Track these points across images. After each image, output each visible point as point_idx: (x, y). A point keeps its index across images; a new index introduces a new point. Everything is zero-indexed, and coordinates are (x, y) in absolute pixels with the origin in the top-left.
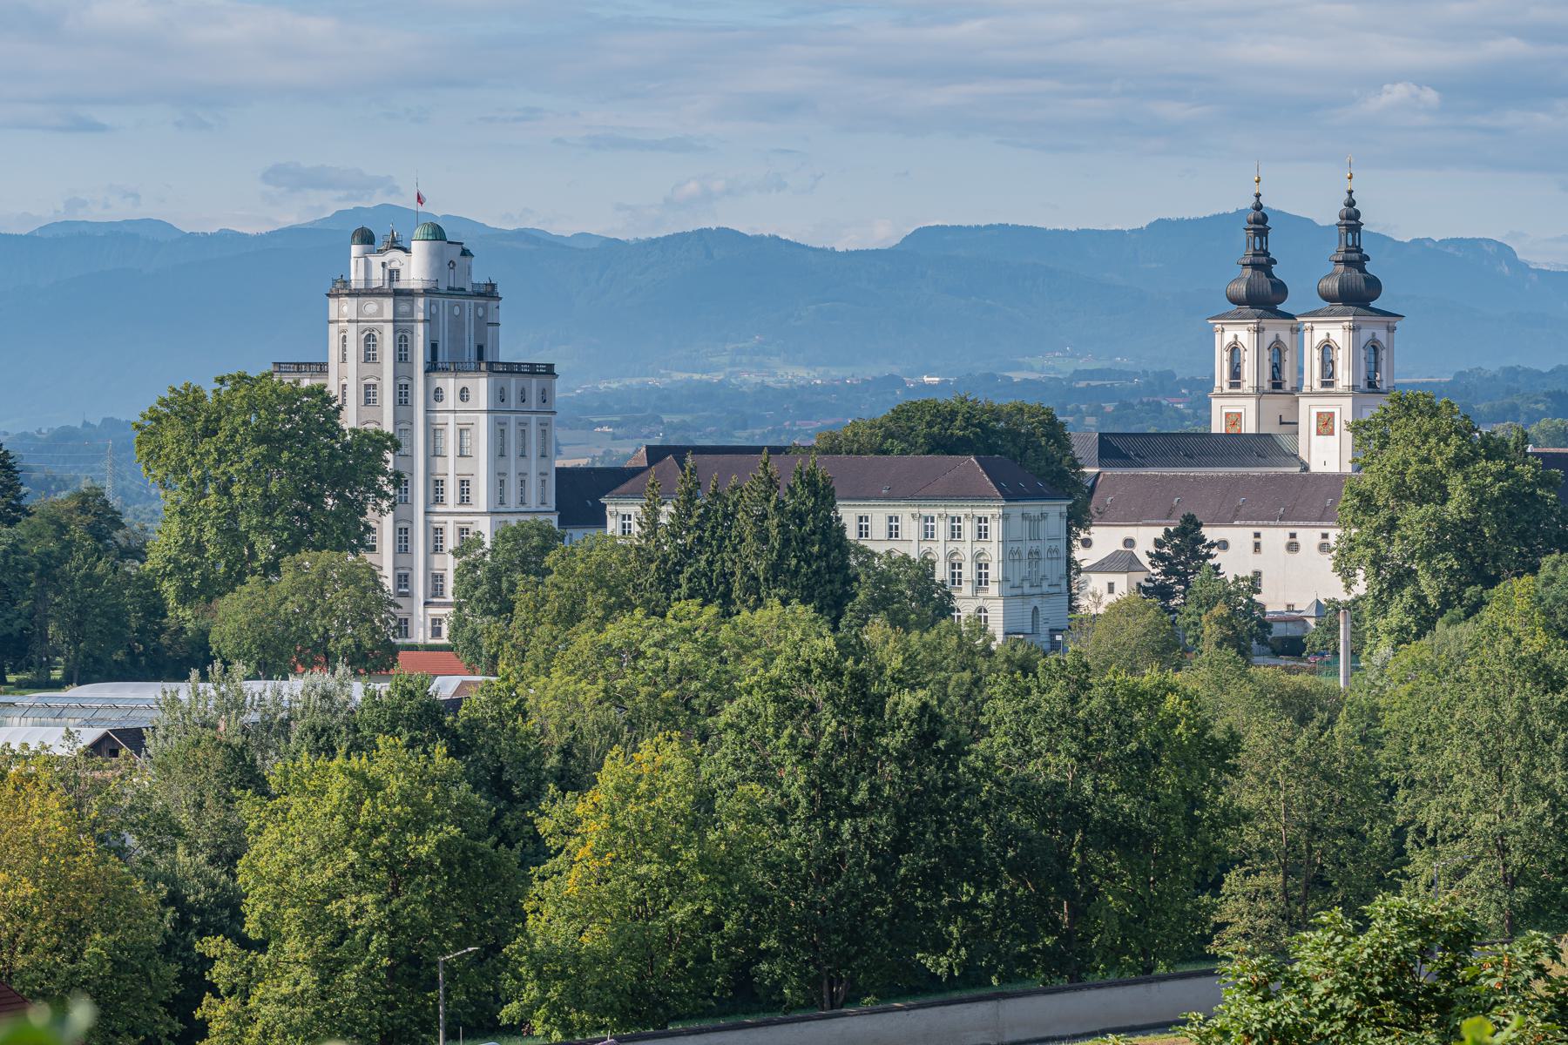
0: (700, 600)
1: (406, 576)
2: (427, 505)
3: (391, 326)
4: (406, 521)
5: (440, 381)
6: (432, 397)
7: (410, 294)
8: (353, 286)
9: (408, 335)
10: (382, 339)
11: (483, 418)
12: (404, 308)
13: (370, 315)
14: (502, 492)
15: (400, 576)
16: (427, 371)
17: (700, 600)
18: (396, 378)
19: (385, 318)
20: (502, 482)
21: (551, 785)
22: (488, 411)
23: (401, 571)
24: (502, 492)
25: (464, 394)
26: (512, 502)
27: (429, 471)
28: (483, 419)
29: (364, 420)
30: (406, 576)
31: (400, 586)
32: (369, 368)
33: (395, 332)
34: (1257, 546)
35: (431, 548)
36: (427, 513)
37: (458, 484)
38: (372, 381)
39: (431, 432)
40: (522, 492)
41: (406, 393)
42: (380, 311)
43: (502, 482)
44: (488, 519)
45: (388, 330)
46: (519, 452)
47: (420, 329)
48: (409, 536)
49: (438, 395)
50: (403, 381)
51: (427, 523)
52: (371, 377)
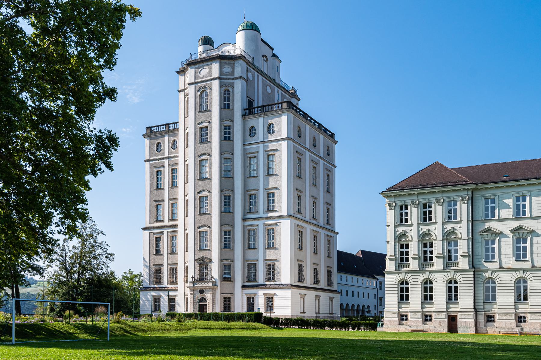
1: (230, 266)
2: (244, 214)
3: (217, 81)
4: (229, 225)
5: (252, 121)
6: (247, 133)
7: (232, 59)
8: (209, 310)
10: (211, 92)
11: (285, 144)
12: (227, 69)
13: (203, 78)
16: (244, 116)
19: (213, 77)
20: (299, 197)
21: (37, 119)
22: (288, 139)
24: (299, 204)
25: (270, 129)
26: (307, 213)
27: (245, 189)
28: (284, 146)
29: (199, 153)
31: (225, 274)
32: (203, 116)
33: (221, 86)
34: (358, 281)
35: (247, 246)
36: (244, 219)
38: (205, 193)
39: (247, 160)
40: (314, 210)
42: (210, 73)
43: (299, 197)
45: (216, 85)
46: (312, 182)
49: (252, 131)
50: (227, 123)
51: (244, 226)
52: (204, 226)
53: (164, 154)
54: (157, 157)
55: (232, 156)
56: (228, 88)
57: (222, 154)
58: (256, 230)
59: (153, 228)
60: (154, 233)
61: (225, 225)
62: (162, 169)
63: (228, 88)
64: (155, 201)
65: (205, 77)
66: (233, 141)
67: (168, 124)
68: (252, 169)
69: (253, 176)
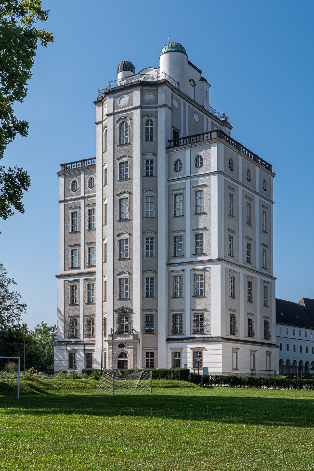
0: (15, 23)
1: (153, 317)
4: (151, 271)
5: (177, 154)
6: (172, 168)
7: (156, 84)
9: (154, 120)
10: (132, 123)
12: (149, 97)
14: (231, 246)
15: (147, 353)
17: (15, 23)
18: (143, 154)
19: (134, 106)
20: (231, 238)
22: (114, 112)
23: (148, 313)
24: (231, 246)
27: (170, 231)
29: (119, 192)
30: (152, 353)
31: (147, 325)
33: (142, 116)
35: (172, 294)
37: (193, 237)
41: (152, 167)
42: (130, 102)
43: (231, 238)
44: (272, 370)
45: (137, 115)
47: (25, 396)
48: (154, 165)
50: (150, 157)
53: (80, 194)
54: (73, 198)
55: (155, 193)
56: (150, 118)
57: (144, 191)
58: (183, 277)
59: (68, 276)
60: (69, 281)
61: (147, 271)
62: (78, 210)
63: (150, 118)
64: (70, 246)
65: (125, 107)
66: (156, 177)
67: (84, 161)
68: (178, 207)
69: (200, 212)
